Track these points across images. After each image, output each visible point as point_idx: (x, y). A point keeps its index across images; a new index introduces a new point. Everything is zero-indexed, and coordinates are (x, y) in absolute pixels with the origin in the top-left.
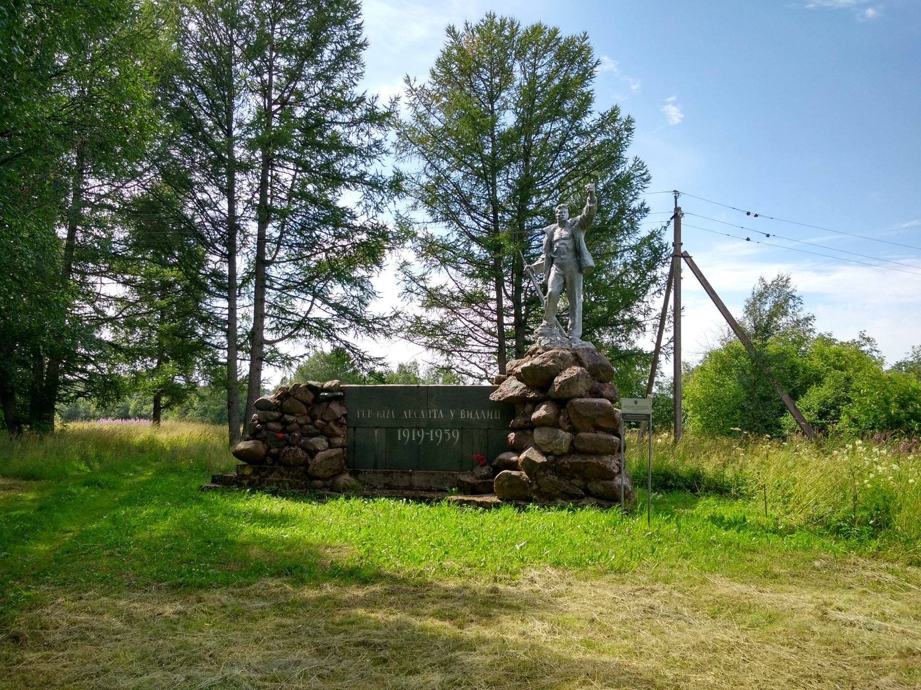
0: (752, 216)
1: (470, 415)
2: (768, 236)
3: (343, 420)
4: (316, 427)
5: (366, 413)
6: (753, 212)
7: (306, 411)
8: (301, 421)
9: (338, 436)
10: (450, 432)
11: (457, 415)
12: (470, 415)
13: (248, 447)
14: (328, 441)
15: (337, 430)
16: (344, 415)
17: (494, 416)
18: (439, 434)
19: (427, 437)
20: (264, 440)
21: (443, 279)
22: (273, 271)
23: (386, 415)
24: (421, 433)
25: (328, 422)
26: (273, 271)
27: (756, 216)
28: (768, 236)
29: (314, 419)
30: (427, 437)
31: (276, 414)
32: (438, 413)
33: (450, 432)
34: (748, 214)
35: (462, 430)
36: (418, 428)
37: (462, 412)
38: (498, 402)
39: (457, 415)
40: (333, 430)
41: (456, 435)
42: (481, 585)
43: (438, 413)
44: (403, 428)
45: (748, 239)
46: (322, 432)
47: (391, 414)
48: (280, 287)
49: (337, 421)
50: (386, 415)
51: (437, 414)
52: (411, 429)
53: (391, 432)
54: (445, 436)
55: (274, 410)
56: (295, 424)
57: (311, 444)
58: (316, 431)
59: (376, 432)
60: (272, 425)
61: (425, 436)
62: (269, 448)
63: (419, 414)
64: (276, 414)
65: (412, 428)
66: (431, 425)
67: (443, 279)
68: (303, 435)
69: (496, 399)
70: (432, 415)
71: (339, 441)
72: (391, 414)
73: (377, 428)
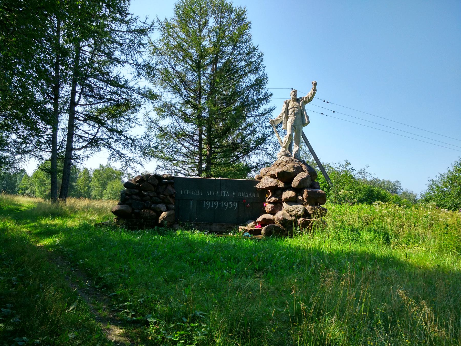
0: (326, 102)
1: (243, 195)
2: (334, 112)
3: (174, 195)
4: (160, 198)
5: (186, 192)
6: (327, 101)
7: (154, 190)
8: (152, 195)
9: (172, 204)
10: (233, 203)
11: (236, 195)
12: (243, 195)
13: (123, 208)
14: (166, 206)
15: (171, 200)
16: (174, 193)
17: (256, 196)
18: (226, 204)
19: (220, 206)
20: (130, 205)
21: (167, 122)
22: (78, 108)
23: (198, 193)
24: (216, 204)
25: (166, 196)
26: (78, 108)
27: (328, 102)
28: (334, 112)
29: (158, 194)
30: (220, 206)
31: (137, 191)
32: (226, 193)
33: (233, 203)
34: (324, 101)
35: (239, 202)
36: (215, 201)
37: (239, 193)
38: (262, 189)
39: (236, 195)
40: (169, 200)
41: (235, 205)
42: (108, 275)
43: (226, 193)
44: (206, 201)
45: (322, 114)
46: (163, 202)
47: (200, 193)
48: (82, 119)
49: (171, 196)
50: (198, 193)
51: (226, 194)
52: (211, 201)
53: (200, 202)
54: (229, 205)
55: (136, 189)
56: (148, 197)
57: (158, 208)
58: (161, 201)
59: (191, 202)
60: (135, 197)
61: (219, 205)
62: (133, 209)
63: (215, 193)
64: (137, 191)
65: (212, 201)
66: (222, 199)
67: (167, 122)
68: (153, 203)
69: (261, 187)
70: (223, 194)
71: (172, 206)
72: (200, 193)
73: (192, 200)
